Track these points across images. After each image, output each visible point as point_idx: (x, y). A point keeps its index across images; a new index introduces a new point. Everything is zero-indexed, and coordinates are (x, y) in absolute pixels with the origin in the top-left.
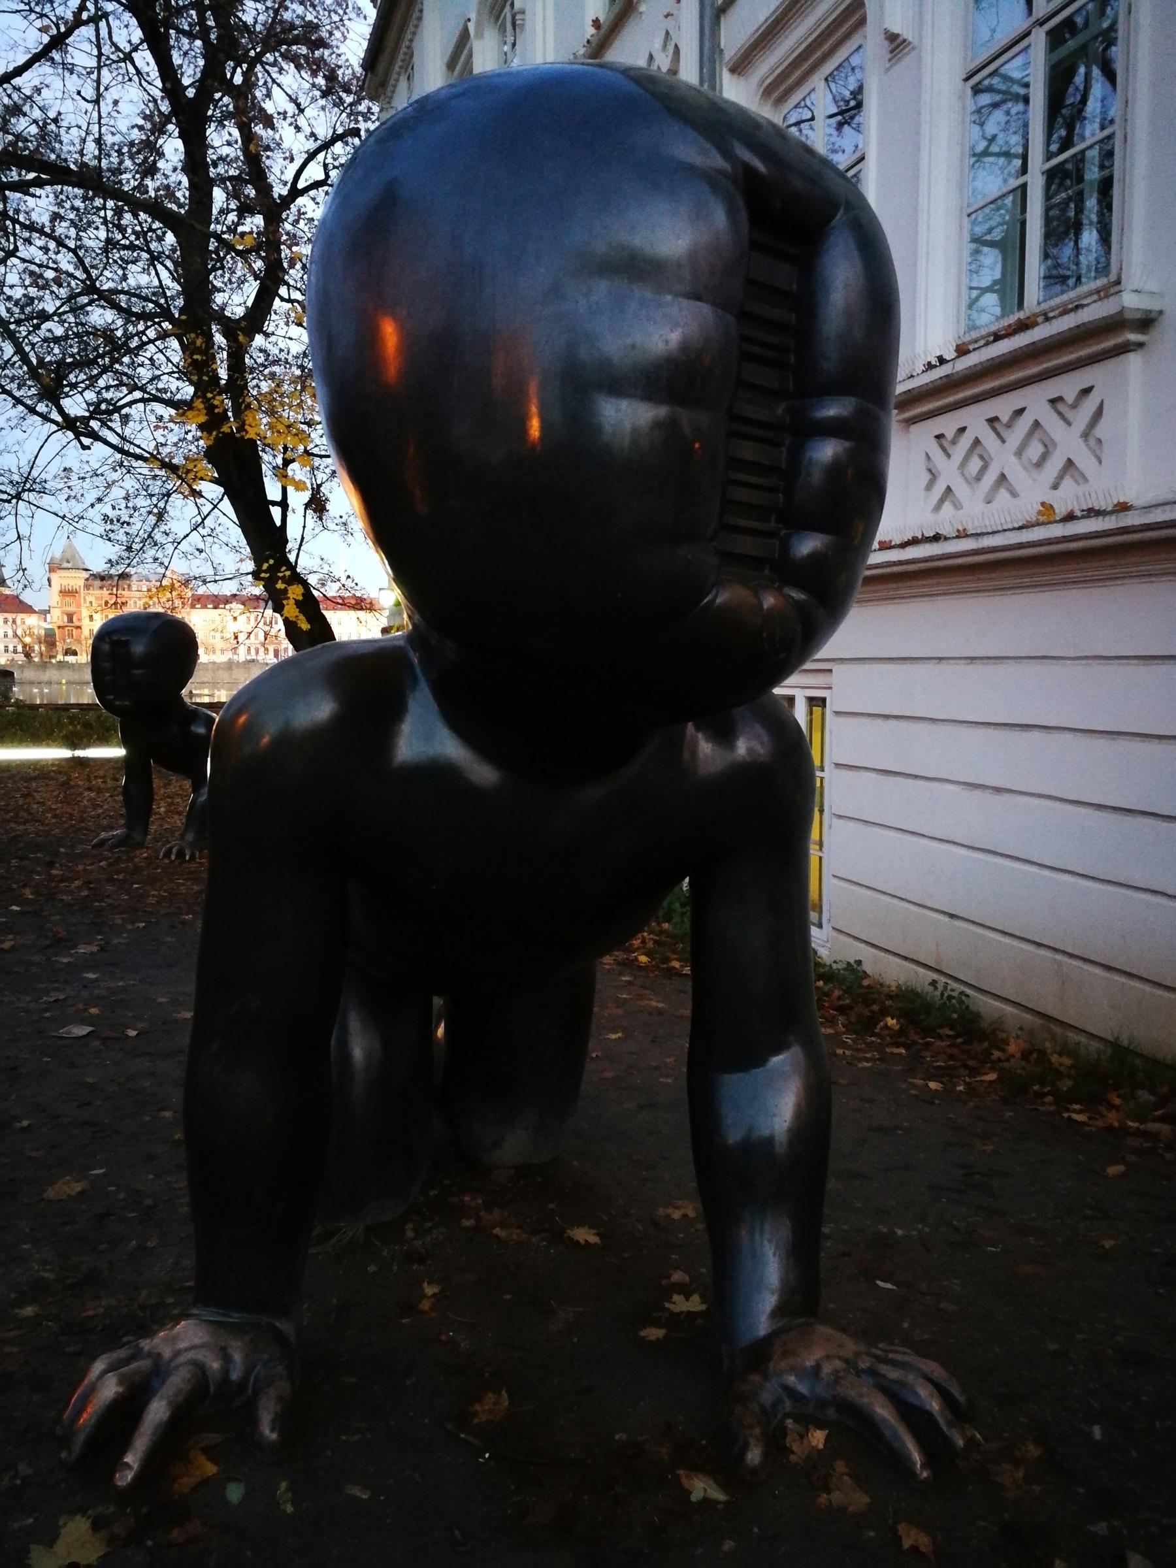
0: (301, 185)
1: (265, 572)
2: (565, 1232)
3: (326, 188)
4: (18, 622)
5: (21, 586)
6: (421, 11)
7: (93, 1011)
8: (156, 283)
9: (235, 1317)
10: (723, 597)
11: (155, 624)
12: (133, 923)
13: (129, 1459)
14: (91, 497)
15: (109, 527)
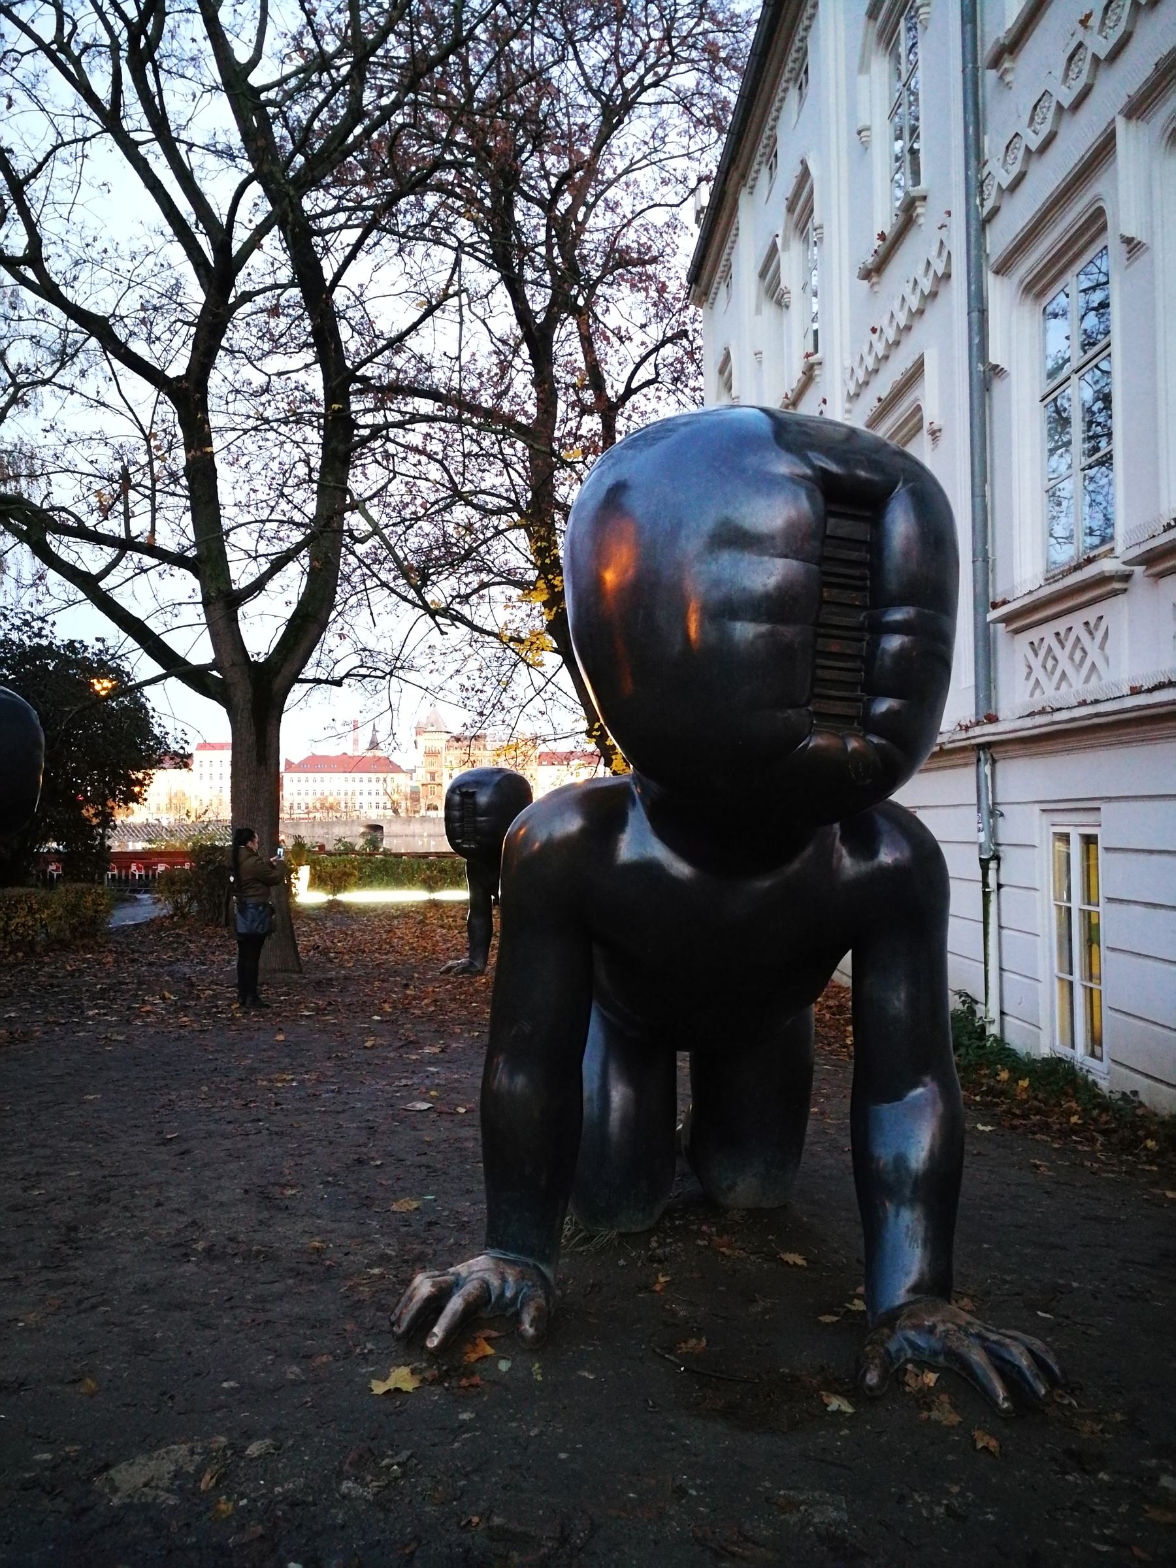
0: (634, 385)
1: (597, 730)
2: (778, 1253)
3: (656, 385)
4: (388, 780)
5: (391, 748)
6: (737, 229)
7: (433, 1093)
8: (508, 482)
9: (511, 1256)
10: (816, 741)
11: (497, 778)
12: (469, 1032)
13: (436, 1330)
14: (451, 668)
15: (464, 694)
